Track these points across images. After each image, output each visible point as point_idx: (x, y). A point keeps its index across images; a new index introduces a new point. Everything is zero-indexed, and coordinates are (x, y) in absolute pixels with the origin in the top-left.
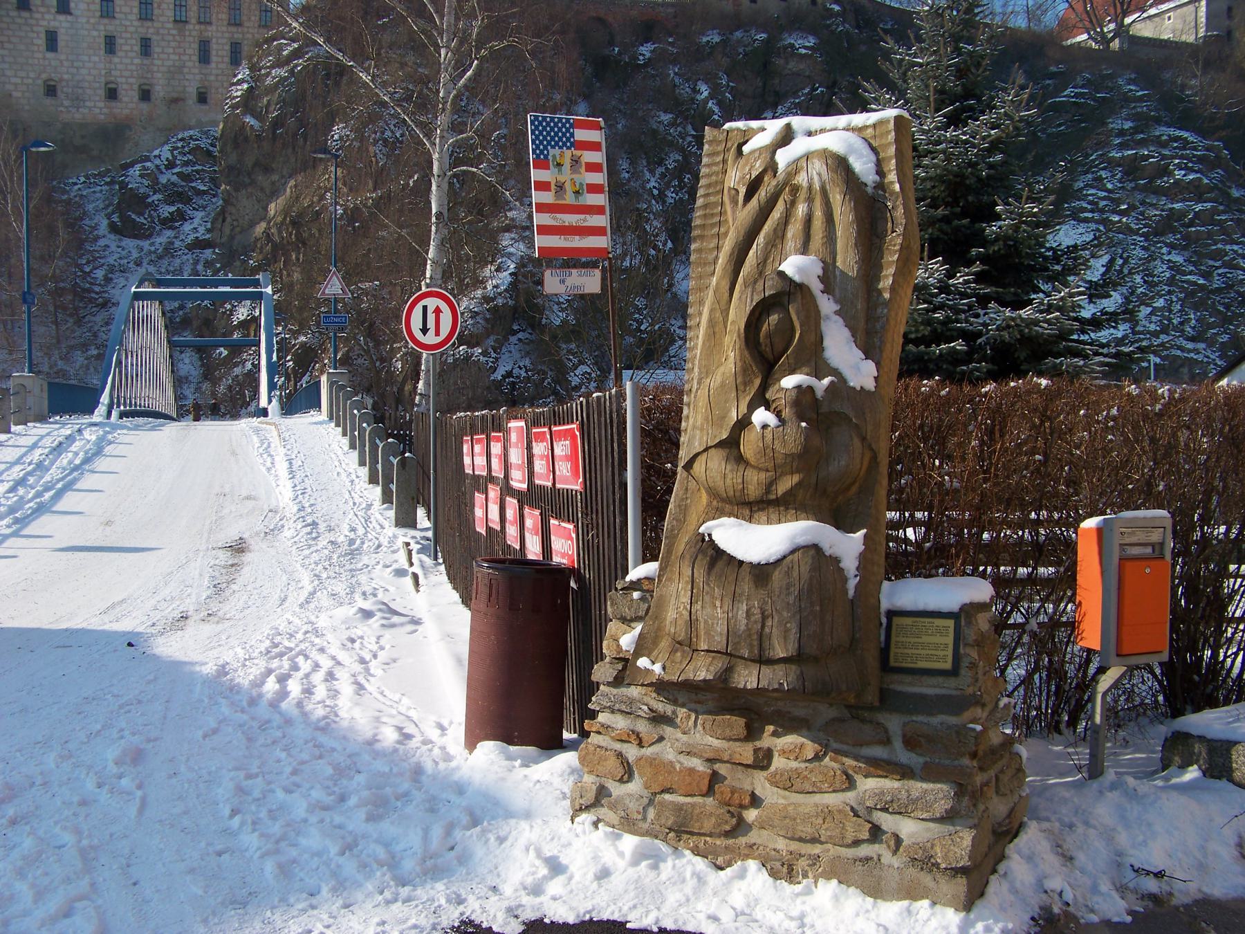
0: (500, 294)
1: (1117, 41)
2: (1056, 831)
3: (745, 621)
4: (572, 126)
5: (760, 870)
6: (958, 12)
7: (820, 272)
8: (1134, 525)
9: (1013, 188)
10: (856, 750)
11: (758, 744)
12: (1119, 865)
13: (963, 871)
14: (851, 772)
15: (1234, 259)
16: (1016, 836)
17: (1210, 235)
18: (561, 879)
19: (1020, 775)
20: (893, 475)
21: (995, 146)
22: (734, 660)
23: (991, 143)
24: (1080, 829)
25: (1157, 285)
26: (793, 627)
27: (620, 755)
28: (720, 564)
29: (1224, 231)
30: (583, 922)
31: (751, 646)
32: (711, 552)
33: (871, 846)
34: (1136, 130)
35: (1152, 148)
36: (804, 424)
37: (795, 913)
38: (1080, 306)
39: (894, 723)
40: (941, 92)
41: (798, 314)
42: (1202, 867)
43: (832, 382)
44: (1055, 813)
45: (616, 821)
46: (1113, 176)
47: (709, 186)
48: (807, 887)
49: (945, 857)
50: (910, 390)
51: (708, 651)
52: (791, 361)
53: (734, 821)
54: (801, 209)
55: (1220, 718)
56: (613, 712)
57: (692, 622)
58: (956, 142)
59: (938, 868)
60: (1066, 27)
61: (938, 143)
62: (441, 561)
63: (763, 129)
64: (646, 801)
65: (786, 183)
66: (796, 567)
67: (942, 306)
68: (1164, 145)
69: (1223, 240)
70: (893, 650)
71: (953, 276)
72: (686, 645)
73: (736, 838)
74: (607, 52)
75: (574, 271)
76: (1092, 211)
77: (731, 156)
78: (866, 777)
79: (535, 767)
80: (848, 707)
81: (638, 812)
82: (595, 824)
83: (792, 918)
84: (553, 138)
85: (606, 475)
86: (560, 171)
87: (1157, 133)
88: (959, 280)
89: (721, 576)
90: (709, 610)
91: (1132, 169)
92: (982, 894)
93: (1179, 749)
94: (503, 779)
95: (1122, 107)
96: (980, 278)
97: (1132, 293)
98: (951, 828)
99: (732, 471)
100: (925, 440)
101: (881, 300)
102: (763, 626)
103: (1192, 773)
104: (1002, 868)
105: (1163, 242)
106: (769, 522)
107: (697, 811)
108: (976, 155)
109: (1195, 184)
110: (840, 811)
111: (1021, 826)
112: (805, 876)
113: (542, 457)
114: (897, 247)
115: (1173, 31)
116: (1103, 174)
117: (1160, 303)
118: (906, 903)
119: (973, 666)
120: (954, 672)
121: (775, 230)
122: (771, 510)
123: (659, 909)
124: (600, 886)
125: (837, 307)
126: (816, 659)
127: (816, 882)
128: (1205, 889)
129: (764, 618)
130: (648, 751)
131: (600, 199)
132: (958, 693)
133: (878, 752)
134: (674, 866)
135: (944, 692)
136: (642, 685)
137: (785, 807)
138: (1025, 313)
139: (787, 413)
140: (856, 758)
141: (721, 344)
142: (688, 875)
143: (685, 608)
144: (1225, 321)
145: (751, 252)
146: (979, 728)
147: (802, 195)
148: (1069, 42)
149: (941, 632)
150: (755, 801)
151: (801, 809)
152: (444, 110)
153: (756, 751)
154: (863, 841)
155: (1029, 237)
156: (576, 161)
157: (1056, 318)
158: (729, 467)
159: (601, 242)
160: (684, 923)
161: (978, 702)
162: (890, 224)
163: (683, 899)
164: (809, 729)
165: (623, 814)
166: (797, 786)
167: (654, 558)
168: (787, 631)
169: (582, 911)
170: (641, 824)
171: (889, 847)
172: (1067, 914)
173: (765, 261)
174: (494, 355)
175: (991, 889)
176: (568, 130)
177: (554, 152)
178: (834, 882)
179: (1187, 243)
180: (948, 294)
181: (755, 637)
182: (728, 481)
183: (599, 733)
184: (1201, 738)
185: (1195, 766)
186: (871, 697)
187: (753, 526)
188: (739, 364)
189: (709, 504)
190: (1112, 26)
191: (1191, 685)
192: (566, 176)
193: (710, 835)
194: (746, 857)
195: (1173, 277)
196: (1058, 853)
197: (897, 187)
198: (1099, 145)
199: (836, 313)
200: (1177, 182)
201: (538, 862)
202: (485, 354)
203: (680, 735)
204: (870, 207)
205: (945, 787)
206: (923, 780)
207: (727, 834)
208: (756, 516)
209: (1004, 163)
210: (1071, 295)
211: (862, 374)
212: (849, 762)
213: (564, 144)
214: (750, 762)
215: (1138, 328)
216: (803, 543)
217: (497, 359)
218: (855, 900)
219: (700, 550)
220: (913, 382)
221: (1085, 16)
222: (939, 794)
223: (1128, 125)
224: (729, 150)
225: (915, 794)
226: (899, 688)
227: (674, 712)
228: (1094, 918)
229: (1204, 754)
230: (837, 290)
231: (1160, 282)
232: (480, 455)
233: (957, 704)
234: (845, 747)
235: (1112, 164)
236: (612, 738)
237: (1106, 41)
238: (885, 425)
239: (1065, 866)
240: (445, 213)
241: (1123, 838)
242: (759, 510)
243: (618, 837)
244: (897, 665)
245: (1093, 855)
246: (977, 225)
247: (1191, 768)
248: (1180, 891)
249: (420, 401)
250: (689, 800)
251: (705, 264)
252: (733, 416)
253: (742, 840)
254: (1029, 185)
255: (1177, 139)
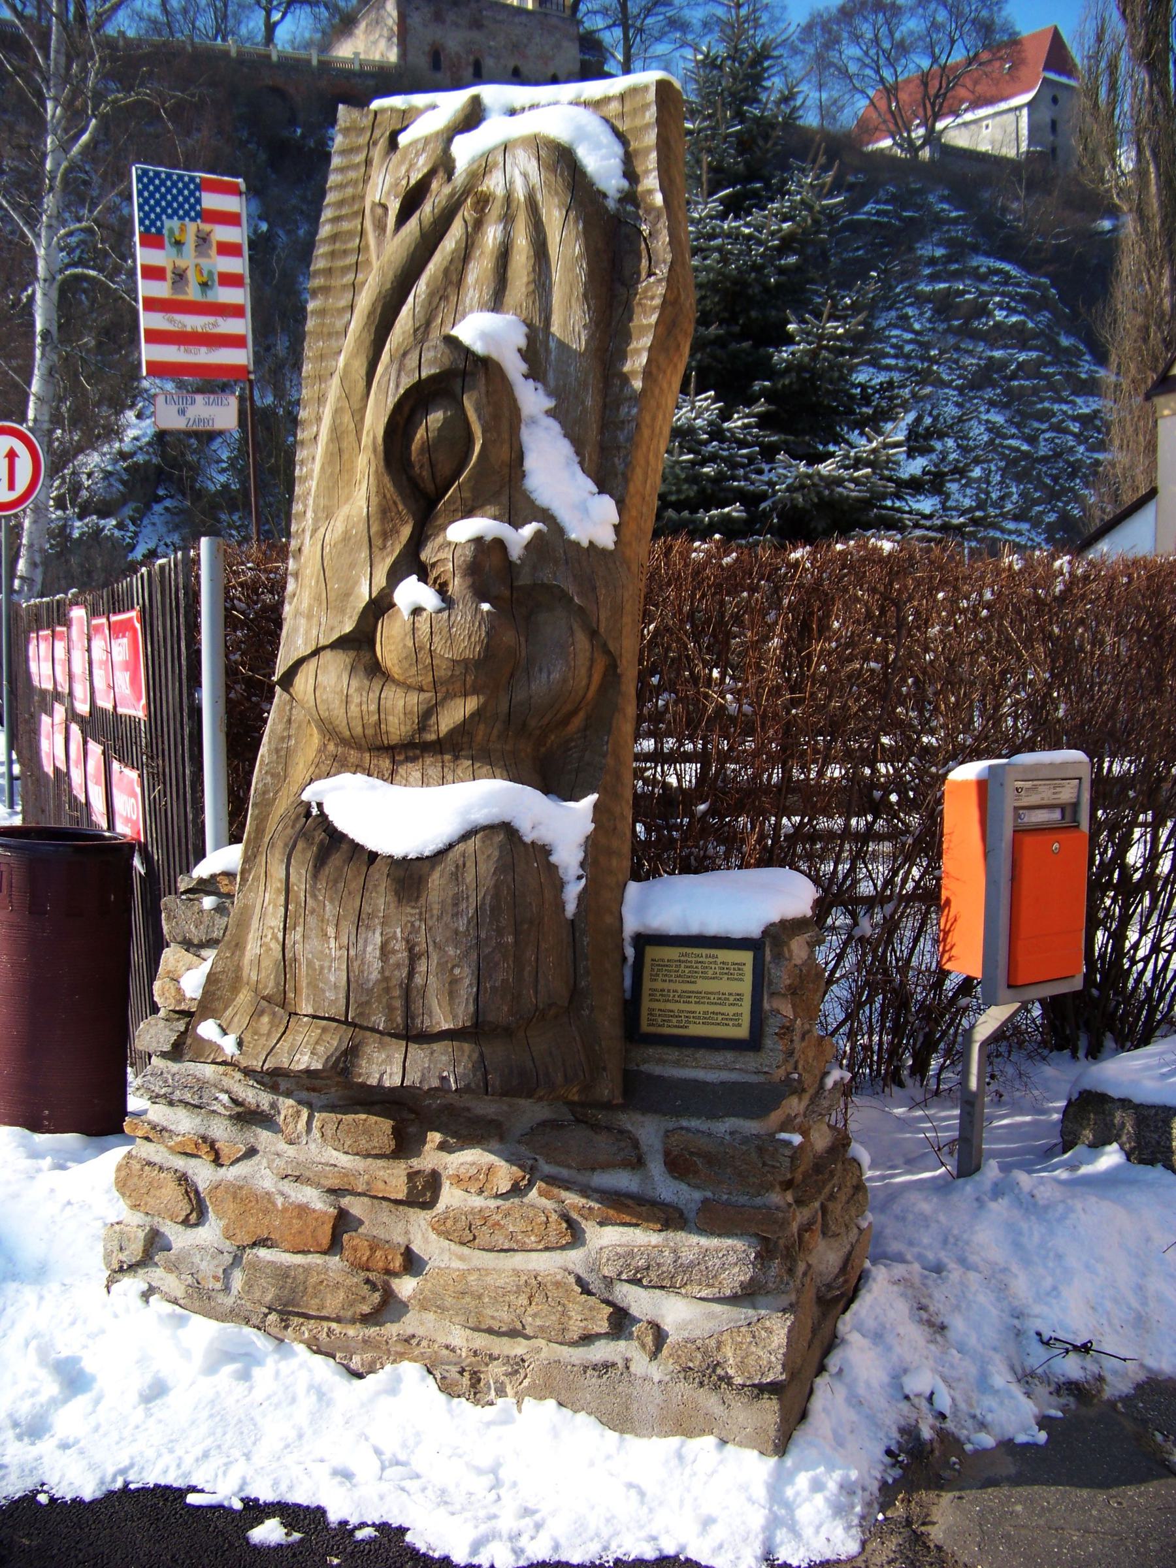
0: (141, 448)
1: (927, 149)
2: (917, 1281)
3: (377, 965)
4: (199, 188)
5: (423, 1379)
6: (741, 63)
7: (522, 342)
8: (1035, 775)
9: (810, 301)
10: (581, 1178)
11: (416, 1163)
12: (1019, 1333)
13: (774, 1388)
14: (575, 1216)
15: (1063, 421)
16: (851, 1300)
17: (1035, 391)
18: (81, 1402)
19: (860, 1196)
20: (644, 693)
21: (787, 244)
22: (360, 1034)
23: (782, 239)
24: (955, 1273)
25: (972, 450)
26: (465, 975)
27: (183, 1179)
28: (336, 860)
29: (1051, 386)
30: (110, 1494)
31: (390, 1008)
32: (320, 836)
33: (613, 1344)
34: (949, 259)
35: (968, 282)
36: (486, 607)
37: (486, 1462)
38: (897, 463)
39: (649, 1131)
40: (715, 170)
41: (478, 410)
42: (1140, 1322)
43: (538, 534)
44: (911, 1243)
45: (179, 1291)
46: (921, 314)
47: (341, 204)
48: (505, 1410)
49: (741, 1366)
50: (675, 555)
51: (314, 1017)
52: (467, 494)
53: (376, 1297)
54: (492, 234)
55: (1148, 1068)
56: (171, 1104)
57: (286, 964)
58: (734, 236)
59: (730, 1384)
60: (867, 130)
61: (712, 236)
62: (19, 808)
63: (434, 107)
64: (228, 1259)
65: (467, 190)
66: (470, 864)
67: (713, 458)
68: (983, 278)
69: (1050, 398)
70: (646, 1004)
71: (728, 418)
72: (279, 1003)
73: (380, 1324)
74: (285, 134)
75: (199, 398)
76: (896, 357)
77: (377, 153)
78: (601, 1224)
79: (75, 1169)
80: (570, 1104)
81: (216, 1278)
82: (146, 1296)
83: (480, 1472)
84: (169, 204)
85: (171, 694)
86: (180, 252)
87: (975, 264)
88: (736, 423)
89: (336, 882)
90: (315, 943)
91: (944, 306)
92: (803, 1416)
93: (1090, 1116)
94: (15, 1196)
95: (933, 230)
96: (764, 421)
97: (943, 460)
98: (751, 1312)
99: (359, 690)
100: (696, 636)
101: (627, 392)
102: (411, 974)
103: (1111, 1158)
104: (834, 1362)
105: (982, 399)
106: (424, 782)
107: (313, 1280)
108: (762, 256)
109: (1019, 328)
110: (557, 1284)
111: (862, 1278)
112: (501, 1392)
113: (101, 662)
114: (657, 302)
115: (992, 143)
116: (910, 311)
117: (977, 472)
118: (675, 1441)
119: (786, 1031)
120: (753, 1043)
121: (446, 271)
122: (428, 760)
123: (248, 1456)
124: (149, 1414)
125: (550, 403)
126: (507, 1032)
127: (519, 1403)
128: (1151, 1362)
129: (413, 958)
130: (231, 1173)
131: (237, 296)
132: (762, 1078)
133: (623, 1180)
134: (277, 1373)
135: (733, 1077)
136: (214, 1062)
137: (463, 1275)
138: (826, 468)
139: (456, 586)
140: (585, 1191)
141: (351, 470)
142: (301, 1388)
143: (274, 937)
144: (1053, 496)
145: (405, 310)
146: (797, 1139)
147: (495, 210)
148: (870, 148)
149: (732, 971)
150: (412, 1263)
151: (489, 1280)
152: (51, 189)
153: (412, 1176)
154: (598, 1336)
155: (831, 368)
156: (203, 240)
157: (866, 477)
158: (355, 683)
159: (239, 357)
160: (290, 1488)
161: (794, 1088)
162: (644, 263)
163: (292, 1435)
164: (502, 1139)
165: (190, 1280)
166: (484, 1238)
167: (235, 839)
168: (454, 982)
169: (111, 1471)
170: (221, 1298)
171: (643, 1346)
172: (943, 1435)
173: (428, 323)
174: (132, 528)
175: (818, 1403)
176: (192, 193)
177: (171, 224)
178: (551, 1403)
179: (1010, 401)
180: (722, 441)
181: (397, 993)
182: (353, 708)
183: (147, 1139)
184: (1125, 1103)
185: (1115, 1146)
186: (609, 1088)
187: (395, 789)
188: (374, 500)
189: (322, 749)
190: (921, 131)
191: (1098, 1013)
192: (188, 259)
193: (338, 1320)
194: (400, 1357)
195: (991, 442)
196: (921, 1321)
197: (658, 199)
198: (904, 275)
199: (550, 413)
200: (998, 325)
201: (44, 1374)
202: (120, 526)
203: (282, 1146)
204: (612, 236)
205: (738, 1244)
206: (702, 1231)
207: (366, 1319)
208: (402, 770)
209: (797, 268)
210: (886, 446)
211: (593, 519)
212: (572, 1199)
213: (187, 214)
214: (401, 1196)
215: (949, 504)
216: (486, 823)
217: (136, 534)
218: (584, 1432)
219: (303, 834)
220: (678, 544)
221: (888, 117)
222: (729, 1255)
223: (939, 252)
224: (375, 144)
225: (687, 1256)
226: (657, 1070)
227: (273, 1105)
228: (988, 1440)
229: (1129, 1128)
230: (551, 376)
231: (976, 447)
232: (46, 660)
233: (757, 1099)
234: (565, 1173)
235: (920, 300)
236: (170, 1148)
237: (913, 149)
238: (632, 608)
239: (933, 1341)
240: (54, 330)
241: (1021, 1286)
242: (409, 759)
243: (181, 1321)
244: (653, 1029)
245: (976, 1321)
246: (762, 350)
247: (1109, 1148)
248: (1115, 1372)
249: (21, 587)
250: (299, 1259)
251: (330, 335)
252: (363, 594)
253: (392, 1330)
254: (833, 298)
255: (997, 272)
